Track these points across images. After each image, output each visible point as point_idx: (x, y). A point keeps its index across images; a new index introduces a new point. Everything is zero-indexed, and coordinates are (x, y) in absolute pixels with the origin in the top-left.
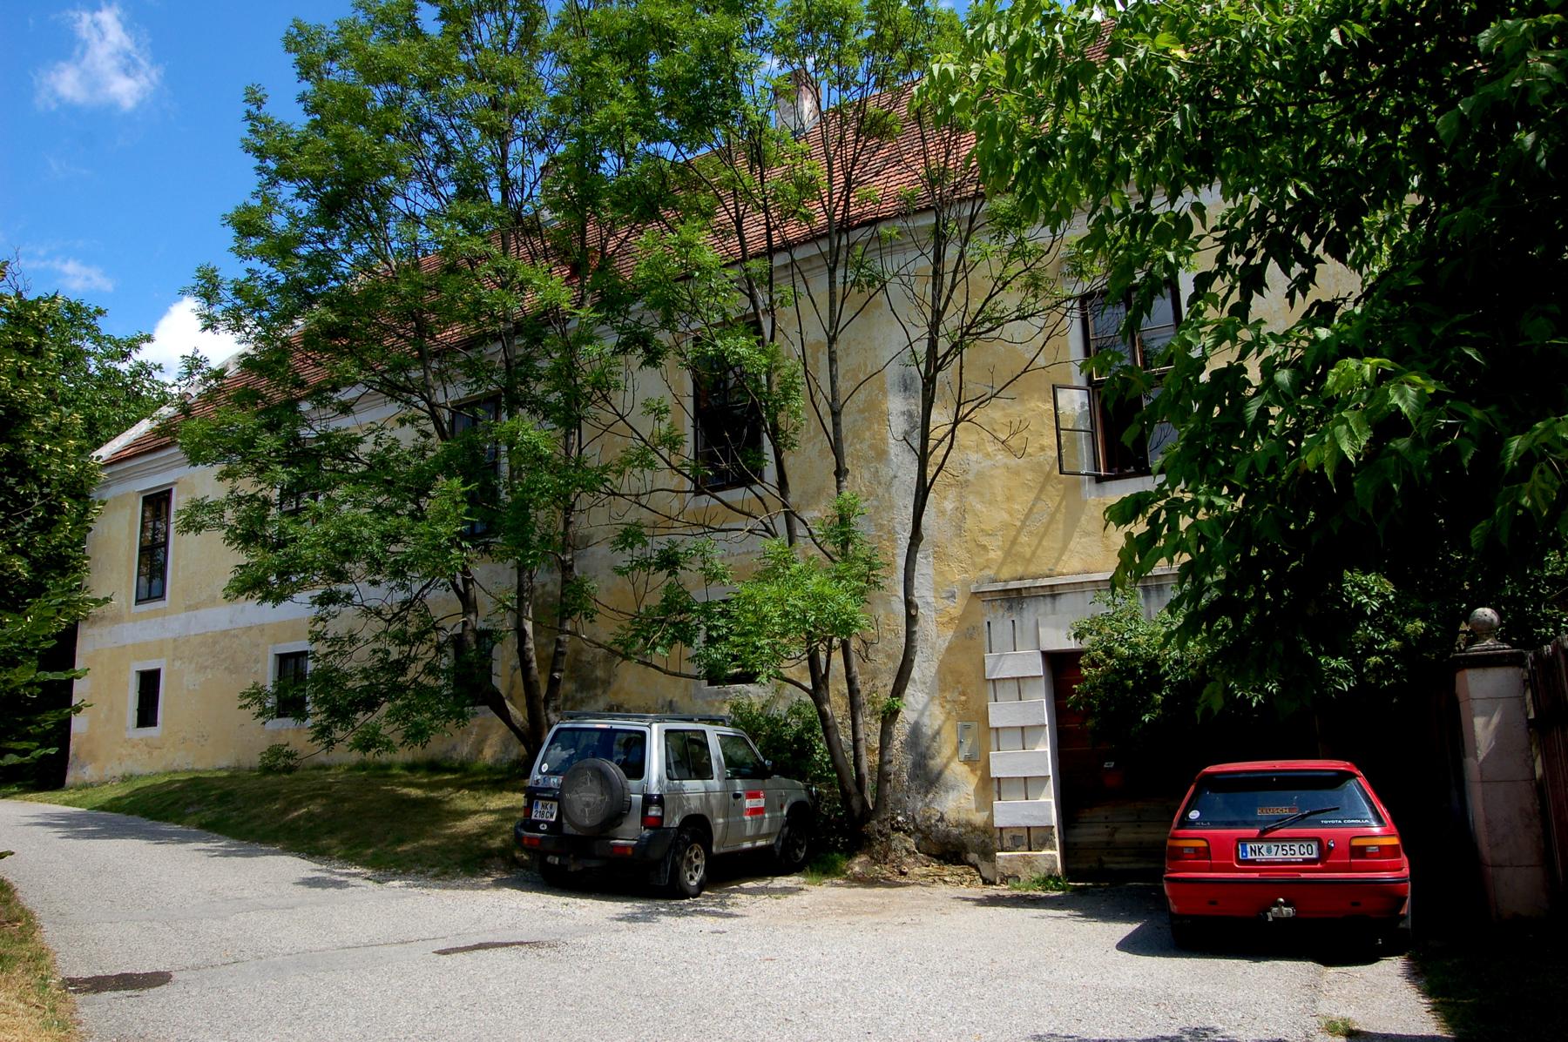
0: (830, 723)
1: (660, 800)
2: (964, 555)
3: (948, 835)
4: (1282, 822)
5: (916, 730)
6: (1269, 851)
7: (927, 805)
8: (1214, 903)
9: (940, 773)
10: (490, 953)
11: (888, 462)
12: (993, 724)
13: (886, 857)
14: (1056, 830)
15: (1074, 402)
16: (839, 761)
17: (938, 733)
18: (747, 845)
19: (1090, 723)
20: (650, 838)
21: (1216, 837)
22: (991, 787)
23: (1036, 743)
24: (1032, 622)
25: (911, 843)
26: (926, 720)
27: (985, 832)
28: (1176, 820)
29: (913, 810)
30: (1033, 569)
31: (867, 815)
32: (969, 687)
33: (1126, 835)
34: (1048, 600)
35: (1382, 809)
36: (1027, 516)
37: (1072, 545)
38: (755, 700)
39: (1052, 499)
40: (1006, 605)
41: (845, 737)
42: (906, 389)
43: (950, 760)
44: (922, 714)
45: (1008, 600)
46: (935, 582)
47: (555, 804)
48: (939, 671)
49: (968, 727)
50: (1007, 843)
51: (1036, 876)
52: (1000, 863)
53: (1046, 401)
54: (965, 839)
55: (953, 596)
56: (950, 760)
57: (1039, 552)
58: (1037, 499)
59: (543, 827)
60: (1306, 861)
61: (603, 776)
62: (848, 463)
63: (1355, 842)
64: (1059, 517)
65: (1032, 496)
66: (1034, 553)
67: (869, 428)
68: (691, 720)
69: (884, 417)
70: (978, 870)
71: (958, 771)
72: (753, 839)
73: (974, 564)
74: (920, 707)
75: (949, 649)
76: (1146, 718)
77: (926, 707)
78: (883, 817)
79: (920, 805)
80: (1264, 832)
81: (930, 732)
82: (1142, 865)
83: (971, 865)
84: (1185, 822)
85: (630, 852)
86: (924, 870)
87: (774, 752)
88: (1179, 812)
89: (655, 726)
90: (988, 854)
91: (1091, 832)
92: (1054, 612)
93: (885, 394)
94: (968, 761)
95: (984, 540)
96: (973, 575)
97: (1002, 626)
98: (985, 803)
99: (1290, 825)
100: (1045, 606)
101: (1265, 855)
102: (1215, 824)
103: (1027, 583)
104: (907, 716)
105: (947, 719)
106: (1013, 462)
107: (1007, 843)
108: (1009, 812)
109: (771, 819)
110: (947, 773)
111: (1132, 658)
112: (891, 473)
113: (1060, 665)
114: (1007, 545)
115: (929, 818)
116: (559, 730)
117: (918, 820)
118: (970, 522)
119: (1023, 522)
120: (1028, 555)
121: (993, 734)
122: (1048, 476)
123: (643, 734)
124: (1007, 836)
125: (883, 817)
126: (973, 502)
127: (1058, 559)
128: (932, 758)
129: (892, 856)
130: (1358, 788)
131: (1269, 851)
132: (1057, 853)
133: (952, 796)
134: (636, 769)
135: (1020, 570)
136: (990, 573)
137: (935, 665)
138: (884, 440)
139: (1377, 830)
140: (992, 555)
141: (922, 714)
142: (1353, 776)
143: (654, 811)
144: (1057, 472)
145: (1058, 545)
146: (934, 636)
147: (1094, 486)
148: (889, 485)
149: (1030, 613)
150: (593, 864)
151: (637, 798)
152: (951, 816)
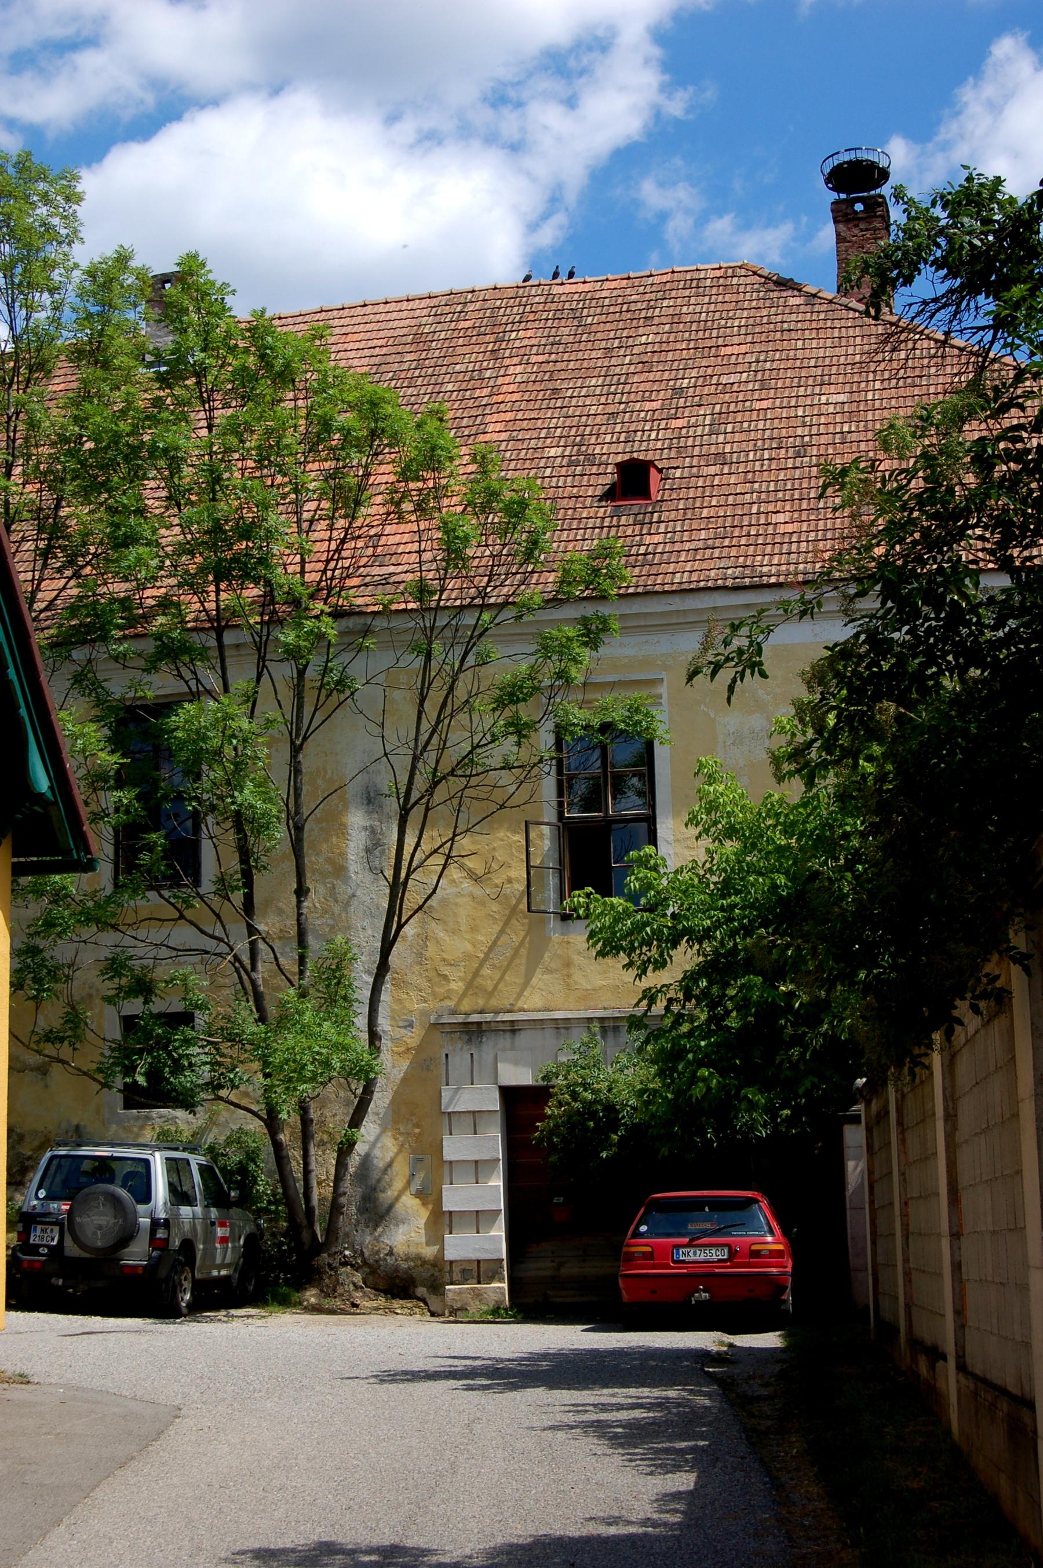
0: (284, 1153)
1: (167, 1223)
2: (425, 984)
3: (397, 1269)
4: (705, 1233)
5: (366, 1161)
6: (695, 1254)
7: (377, 1239)
8: (654, 1292)
9: (391, 1207)
10: (92, 1336)
11: (346, 880)
12: (448, 1156)
13: (335, 1290)
14: (505, 1263)
15: (545, 841)
16: (292, 1192)
17: (390, 1165)
18: (215, 1273)
19: (553, 1159)
20: (160, 1257)
21: (658, 1244)
22: (442, 1221)
23: (489, 1177)
24: (490, 1058)
25: (358, 1278)
26: (377, 1152)
27: (434, 1265)
28: (630, 1233)
29: (361, 1245)
30: (494, 1003)
31: (318, 1248)
32: (424, 1122)
33: (571, 1269)
34: (508, 1035)
35: (774, 1225)
36: (491, 949)
37: (534, 981)
38: (182, 1126)
39: (517, 933)
40: (466, 1037)
41: (296, 1168)
42: (369, 802)
43: (401, 1193)
44: (373, 1145)
45: (467, 1032)
46: (393, 1011)
47: (56, 1229)
48: (393, 1101)
49: (421, 1160)
50: (456, 1276)
51: (485, 1308)
52: (450, 1296)
53: (515, 832)
54: (414, 1274)
55: (411, 1026)
56: (401, 1193)
57: (501, 986)
58: (502, 931)
59: (44, 1251)
60: (720, 1261)
61: (115, 1201)
62: (309, 884)
63: (754, 1247)
64: (523, 951)
65: (497, 928)
66: (496, 987)
67: (327, 840)
68: (176, 1149)
69: (342, 830)
70: (426, 1304)
71: (409, 1203)
72: (219, 1267)
73: (434, 994)
74: (372, 1139)
75: (404, 1080)
76: (604, 1155)
77: (377, 1139)
78: (334, 1249)
79: (368, 1239)
80: (692, 1240)
81: (381, 1165)
82: (585, 1299)
83: (419, 1299)
84: (637, 1234)
85: (140, 1271)
86: (374, 1304)
87: (226, 1185)
88: (632, 1227)
89: (157, 1154)
90: (436, 1288)
91: (538, 1268)
92: (512, 1048)
93: (346, 807)
94: (420, 1194)
95: (446, 970)
96: (432, 1005)
97: (460, 1060)
98: (435, 1235)
99: (710, 1235)
100: (505, 1041)
101: (692, 1257)
102: (658, 1235)
103: (488, 1017)
104: (360, 1148)
105: (400, 1151)
106: (477, 891)
107: (456, 1276)
108: (460, 1246)
109: (233, 1248)
110: (399, 1207)
111: (595, 1102)
112: (350, 891)
113: (519, 1105)
114: (470, 976)
115: (378, 1252)
116: (53, 1158)
117: (367, 1253)
118: (431, 951)
119: (487, 954)
120: (490, 989)
121: (446, 1167)
122: (514, 910)
123: (146, 1163)
124: (456, 1269)
125: (334, 1249)
126: (437, 930)
127: (520, 995)
128: (383, 1191)
129: (340, 1290)
130: (763, 1212)
131: (695, 1254)
132: (505, 1285)
133: (402, 1229)
134: (145, 1195)
135: (481, 1002)
136: (451, 1004)
137: (389, 1095)
138: (343, 854)
139: (769, 1239)
140: (453, 986)
141: (373, 1145)
142: (757, 1201)
143: (161, 1234)
144: (524, 906)
145: (520, 981)
146: (392, 1067)
147: (559, 923)
148: (347, 905)
149: (488, 1048)
150: (100, 1284)
151: (145, 1221)
152: (400, 1249)
